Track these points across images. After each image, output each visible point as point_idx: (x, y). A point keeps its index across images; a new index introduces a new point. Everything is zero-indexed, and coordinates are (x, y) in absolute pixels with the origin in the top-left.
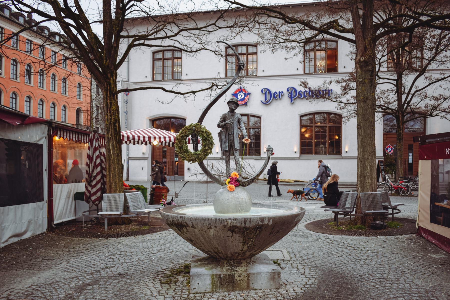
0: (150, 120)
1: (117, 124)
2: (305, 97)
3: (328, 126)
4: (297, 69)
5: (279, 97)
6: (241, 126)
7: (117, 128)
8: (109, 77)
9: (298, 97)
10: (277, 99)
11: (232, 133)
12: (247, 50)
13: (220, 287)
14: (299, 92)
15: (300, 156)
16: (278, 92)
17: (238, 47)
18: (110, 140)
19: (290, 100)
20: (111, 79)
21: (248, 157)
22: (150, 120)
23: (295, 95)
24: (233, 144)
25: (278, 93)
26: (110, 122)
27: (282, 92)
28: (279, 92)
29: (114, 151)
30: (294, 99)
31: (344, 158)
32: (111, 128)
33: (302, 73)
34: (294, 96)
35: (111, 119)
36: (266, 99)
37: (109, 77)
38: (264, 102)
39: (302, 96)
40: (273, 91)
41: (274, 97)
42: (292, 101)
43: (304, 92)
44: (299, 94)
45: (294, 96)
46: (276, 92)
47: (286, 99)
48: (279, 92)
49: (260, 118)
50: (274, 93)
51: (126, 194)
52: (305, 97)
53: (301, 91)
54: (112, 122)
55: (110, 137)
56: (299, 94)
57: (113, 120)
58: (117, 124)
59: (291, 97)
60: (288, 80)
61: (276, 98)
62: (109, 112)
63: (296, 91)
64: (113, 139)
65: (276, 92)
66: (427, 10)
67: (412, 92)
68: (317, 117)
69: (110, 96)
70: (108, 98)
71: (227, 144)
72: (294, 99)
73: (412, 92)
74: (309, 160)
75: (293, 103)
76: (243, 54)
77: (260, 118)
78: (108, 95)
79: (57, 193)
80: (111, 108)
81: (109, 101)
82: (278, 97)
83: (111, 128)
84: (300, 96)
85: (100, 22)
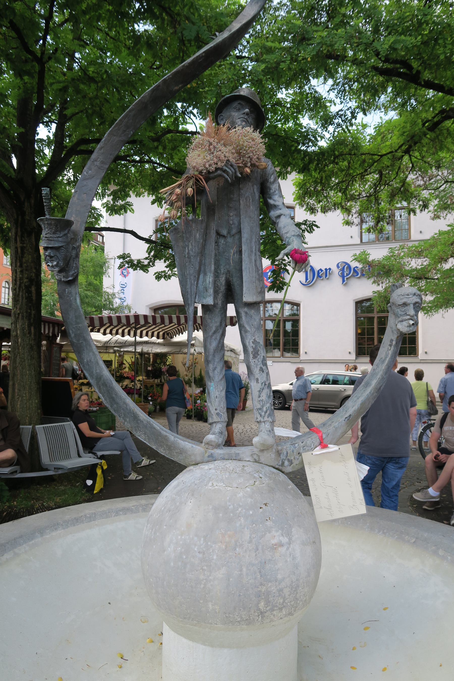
0: (150, 308)
1: (33, 289)
2: (363, 275)
4: (351, 237)
5: (326, 276)
6: (271, 202)
7: (32, 296)
8: (22, 199)
9: (353, 276)
10: (323, 279)
11: (234, 231)
14: (354, 268)
15: (356, 358)
16: (323, 269)
18: (18, 317)
19: (340, 280)
20: (26, 204)
21: (190, 441)
22: (150, 308)
24: (235, 281)
25: (324, 271)
26: (20, 284)
27: (330, 269)
28: (326, 269)
29: (23, 340)
30: (347, 279)
31: (422, 361)
32: (20, 296)
33: (359, 242)
34: (347, 275)
35: (21, 279)
36: (307, 279)
37: (22, 199)
38: (305, 283)
41: (319, 276)
42: (343, 281)
45: (347, 275)
46: (321, 270)
47: (337, 279)
48: (326, 269)
49: (298, 305)
50: (318, 271)
51: (37, 426)
53: (357, 267)
54: (23, 285)
55: (19, 314)
56: (355, 271)
57: (25, 280)
58: (33, 289)
59: (343, 276)
61: (321, 277)
62: (18, 264)
63: (349, 267)
64: (23, 316)
65: (321, 270)
69: (22, 236)
70: (18, 239)
71: (210, 279)
72: (347, 279)
75: (346, 283)
77: (298, 305)
78: (19, 233)
80: (22, 257)
81: (19, 245)
82: (324, 276)
83: (20, 296)
84: (355, 274)
85: (148, 241)
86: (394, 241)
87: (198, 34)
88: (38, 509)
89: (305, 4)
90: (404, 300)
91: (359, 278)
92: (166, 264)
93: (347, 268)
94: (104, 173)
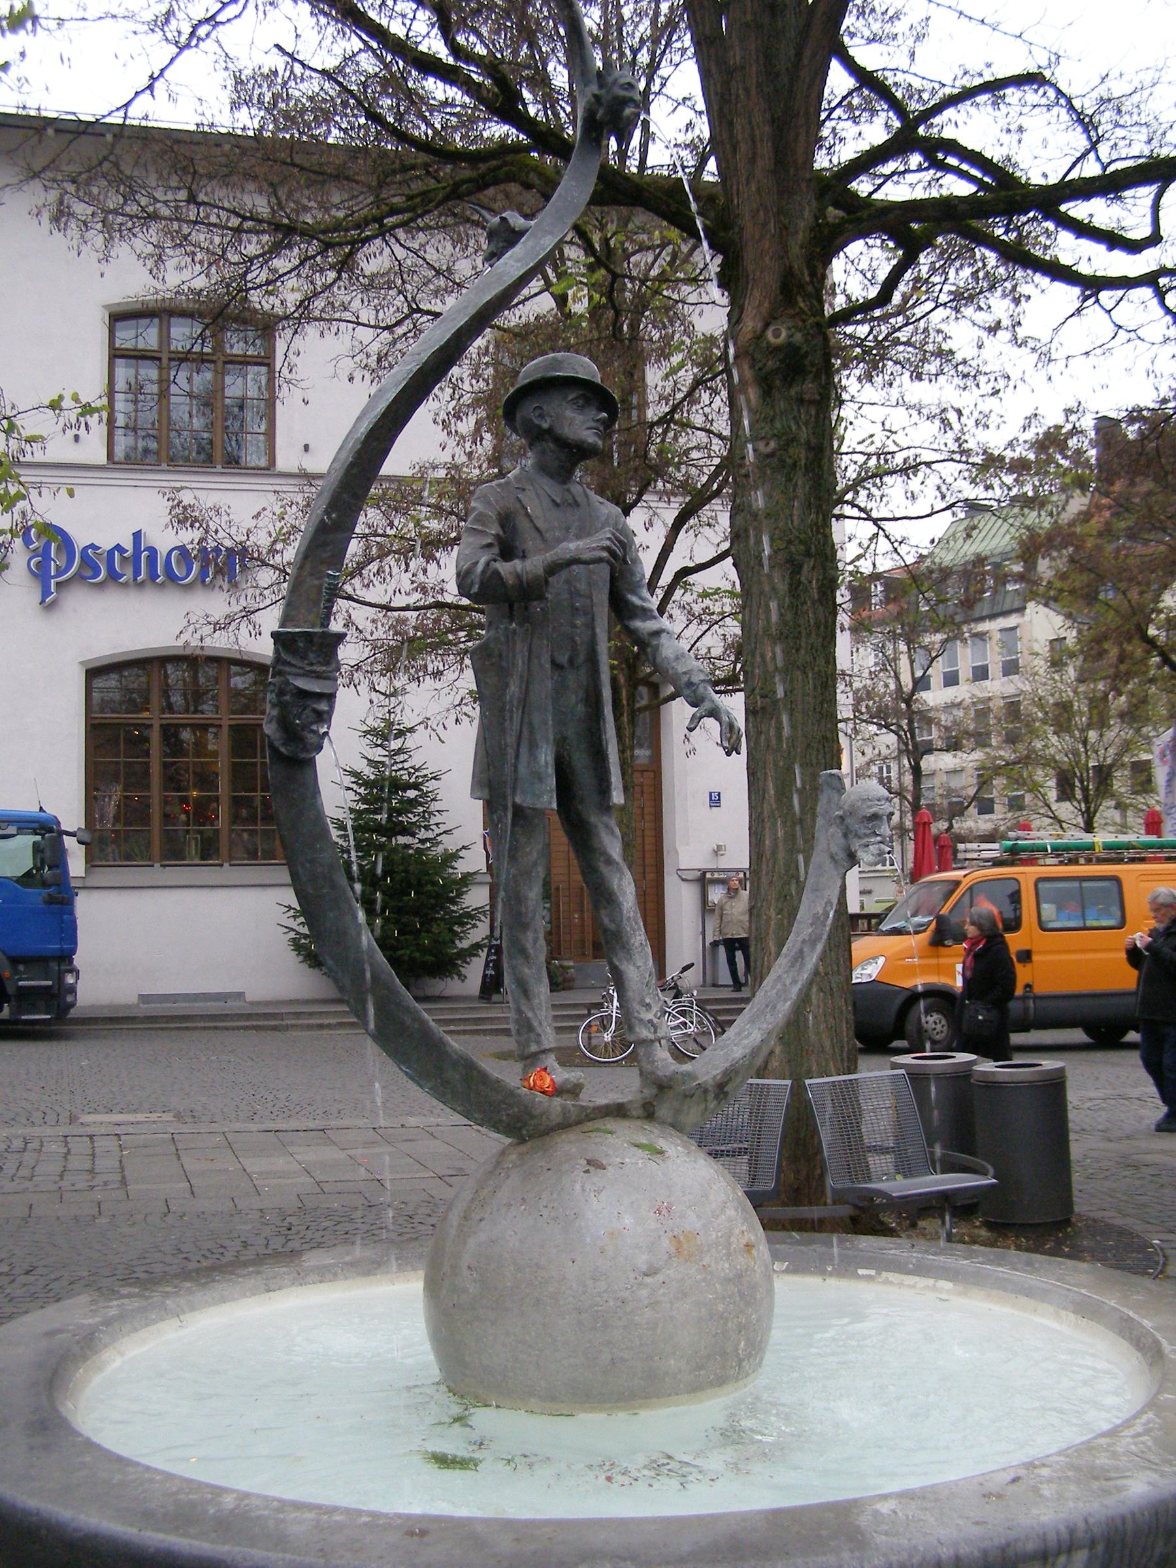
2: (113, 576)
3: (226, 723)
9: (79, 577)
12: (165, 338)
13: (1094, 1456)
17: (173, 320)
23: (62, 562)
24: (580, 761)
30: (58, 584)
33: (102, 459)
34: (60, 572)
39: (97, 573)
40: (81, 540)
42: (46, 593)
43: (111, 553)
44: (86, 560)
45: (60, 572)
52: (113, 576)
53: (93, 546)
56: (86, 560)
59: (41, 574)
60: (86, 488)
66: (758, 211)
67: (666, 578)
68: (175, 674)
72: (58, 584)
73: (666, 578)
74: (135, 894)
76: (183, 358)
79: (948, 956)
84: (89, 573)
86: (164, 466)
87: (985, 328)
88: (828, 662)
89: (852, 347)
90: (874, 810)
91: (101, 586)
92: (354, 805)
93: (58, 549)
94: (628, 875)
